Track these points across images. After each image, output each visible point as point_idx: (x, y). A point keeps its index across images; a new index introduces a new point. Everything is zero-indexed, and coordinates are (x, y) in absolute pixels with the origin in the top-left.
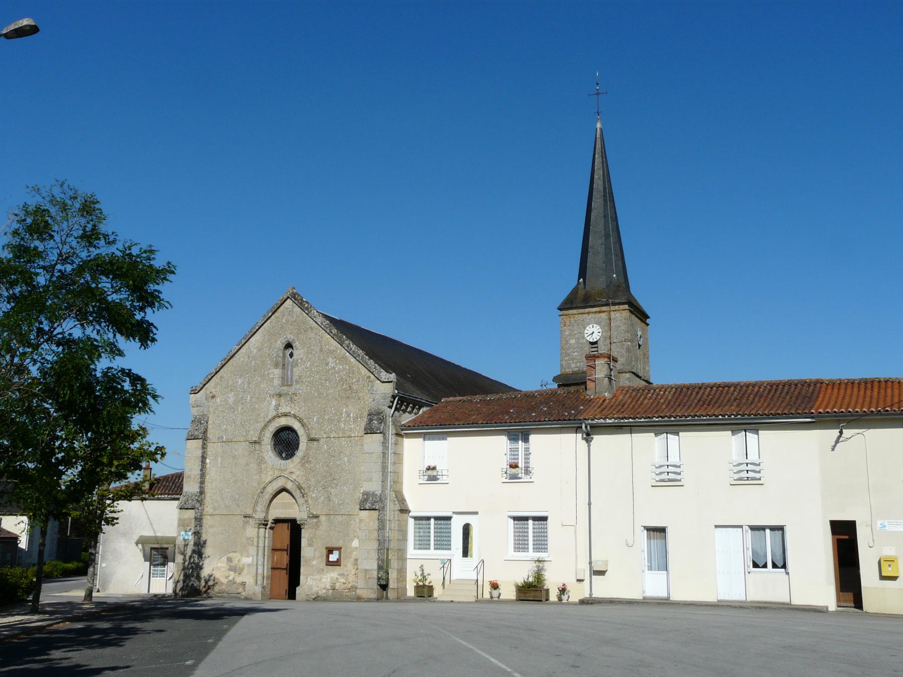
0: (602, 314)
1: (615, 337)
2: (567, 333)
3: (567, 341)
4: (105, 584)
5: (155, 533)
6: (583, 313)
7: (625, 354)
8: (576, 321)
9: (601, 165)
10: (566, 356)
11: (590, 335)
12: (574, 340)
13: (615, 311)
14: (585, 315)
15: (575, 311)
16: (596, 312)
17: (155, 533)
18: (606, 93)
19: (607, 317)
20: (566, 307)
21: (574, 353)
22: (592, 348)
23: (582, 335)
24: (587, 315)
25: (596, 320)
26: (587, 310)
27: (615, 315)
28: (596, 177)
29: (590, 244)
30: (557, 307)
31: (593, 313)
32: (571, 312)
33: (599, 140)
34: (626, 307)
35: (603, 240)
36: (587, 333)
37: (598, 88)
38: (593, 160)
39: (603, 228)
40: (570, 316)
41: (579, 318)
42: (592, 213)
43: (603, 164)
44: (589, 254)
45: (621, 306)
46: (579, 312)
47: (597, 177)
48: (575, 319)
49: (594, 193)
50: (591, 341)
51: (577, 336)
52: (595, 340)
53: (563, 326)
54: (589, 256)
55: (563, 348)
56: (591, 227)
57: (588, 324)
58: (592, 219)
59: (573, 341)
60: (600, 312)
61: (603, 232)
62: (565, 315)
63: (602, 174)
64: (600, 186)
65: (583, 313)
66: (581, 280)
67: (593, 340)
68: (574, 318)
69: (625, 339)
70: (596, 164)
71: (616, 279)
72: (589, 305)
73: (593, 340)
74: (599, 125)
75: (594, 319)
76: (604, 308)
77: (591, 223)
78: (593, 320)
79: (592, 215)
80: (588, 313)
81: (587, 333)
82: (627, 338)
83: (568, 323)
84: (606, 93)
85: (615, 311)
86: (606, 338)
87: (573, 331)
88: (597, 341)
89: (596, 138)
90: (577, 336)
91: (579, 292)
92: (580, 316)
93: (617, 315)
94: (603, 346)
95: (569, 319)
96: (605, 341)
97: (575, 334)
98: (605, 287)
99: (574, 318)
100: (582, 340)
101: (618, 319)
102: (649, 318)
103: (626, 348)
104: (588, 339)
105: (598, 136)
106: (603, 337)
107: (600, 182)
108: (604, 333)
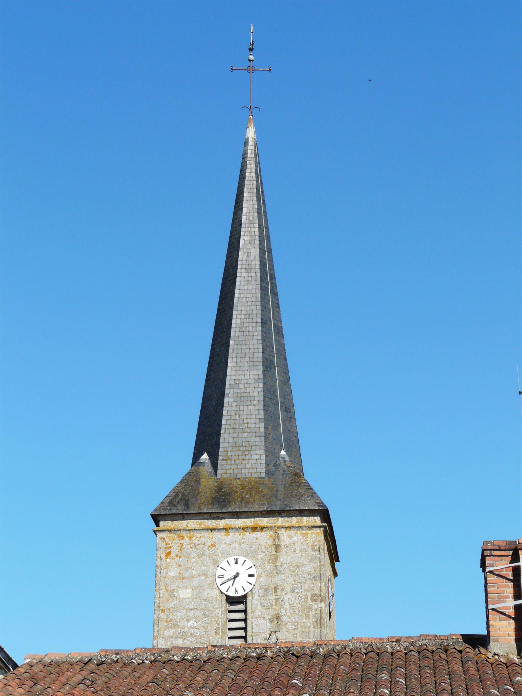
0: (258, 534)
1: (289, 590)
2: (172, 574)
3: (172, 591)
4: (243, 608)
5: (510, 556)
6: (212, 530)
7: (312, 629)
8: (195, 545)
9: (256, 214)
10: (168, 628)
11: (229, 580)
12: (189, 590)
13: (291, 527)
14: (217, 534)
15: (193, 524)
16: (245, 529)
17: (510, 556)
18: (270, 70)
19: (270, 542)
20: (174, 512)
21: (188, 621)
22: (230, 612)
23: (209, 580)
24: (223, 533)
25: (245, 546)
26: (222, 523)
27: (291, 537)
28: (244, 239)
29: (228, 378)
30: (150, 513)
31: (238, 529)
32: (183, 524)
33: (253, 163)
34: (317, 520)
35: (261, 372)
36: (223, 576)
37: (251, 57)
38: (236, 203)
39: (260, 346)
40: (183, 533)
41: (202, 540)
42: (234, 313)
43: (259, 213)
44: (226, 399)
45: (305, 519)
46: (203, 526)
47: (246, 238)
48: (195, 540)
49: (239, 271)
50: (232, 593)
51: (196, 582)
52: (241, 593)
53: (163, 556)
54: (225, 404)
55: (162, 608)
56: (231, 342)
57: (226, 555)
58: (233, 325)
59: (185, 593)
60: (254, 529)
61: (260, 355)
62: (170, 531)
63: (257, 234)
64: (252, 258)
65: (212, 530)
66: (205, 457)
67: (236, 591)
68: (190, 538)
69: (313, 595)
70: (244, 211)
71: (287, 458)
72: (229, 510)
73: (236, 591)
74: (251, 133)
75: (240, 544)
76: (264, 521)
77: (232, 334)
78: (237, 545)
79: (234, 317)
80: (226, 529)
81: (223, 576)
82: (318, 592)
83: (175, 550)
84: (270, 70)
85: (291, 527)
86: (266, 590)
87: (187, 569)
88: (245, 596)
89: (244, 158)
90: (196, 582)
91: (203, 481)
92: (206, 534)
93: (295, 538)
94: (259, 608)
95: (177, 541)
96: (264, 596)
97: (192, 577)
98: (263, 475)
99: (190, 538)
100: (209, 591)
101: (296, 546)
102: (339, 561)
103: (315, 616)
104: (224, 588)
105: (249, 155)
106: (261, 588)
107: (253, 250)
108: (262, 579)
